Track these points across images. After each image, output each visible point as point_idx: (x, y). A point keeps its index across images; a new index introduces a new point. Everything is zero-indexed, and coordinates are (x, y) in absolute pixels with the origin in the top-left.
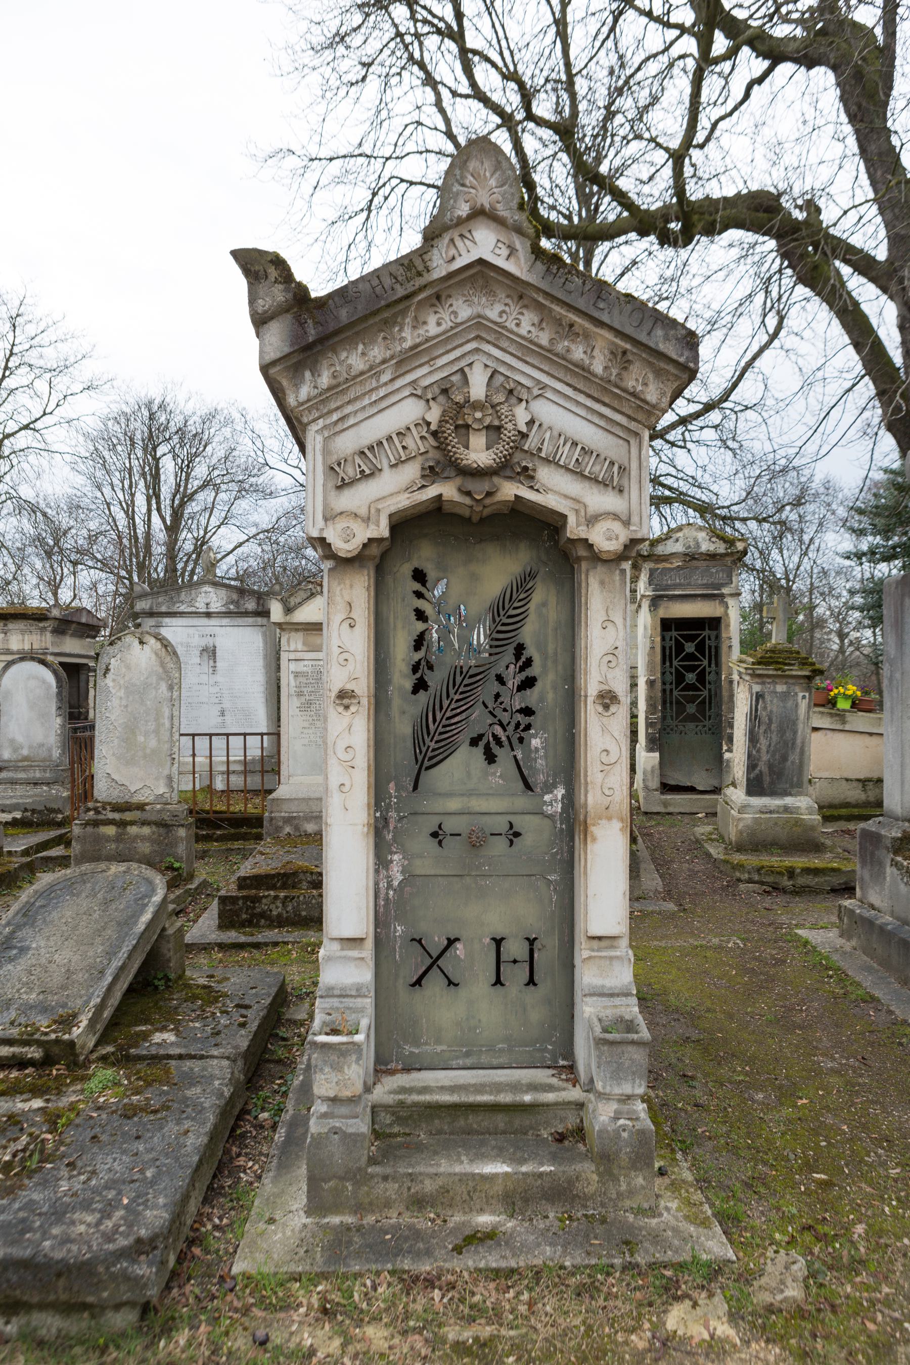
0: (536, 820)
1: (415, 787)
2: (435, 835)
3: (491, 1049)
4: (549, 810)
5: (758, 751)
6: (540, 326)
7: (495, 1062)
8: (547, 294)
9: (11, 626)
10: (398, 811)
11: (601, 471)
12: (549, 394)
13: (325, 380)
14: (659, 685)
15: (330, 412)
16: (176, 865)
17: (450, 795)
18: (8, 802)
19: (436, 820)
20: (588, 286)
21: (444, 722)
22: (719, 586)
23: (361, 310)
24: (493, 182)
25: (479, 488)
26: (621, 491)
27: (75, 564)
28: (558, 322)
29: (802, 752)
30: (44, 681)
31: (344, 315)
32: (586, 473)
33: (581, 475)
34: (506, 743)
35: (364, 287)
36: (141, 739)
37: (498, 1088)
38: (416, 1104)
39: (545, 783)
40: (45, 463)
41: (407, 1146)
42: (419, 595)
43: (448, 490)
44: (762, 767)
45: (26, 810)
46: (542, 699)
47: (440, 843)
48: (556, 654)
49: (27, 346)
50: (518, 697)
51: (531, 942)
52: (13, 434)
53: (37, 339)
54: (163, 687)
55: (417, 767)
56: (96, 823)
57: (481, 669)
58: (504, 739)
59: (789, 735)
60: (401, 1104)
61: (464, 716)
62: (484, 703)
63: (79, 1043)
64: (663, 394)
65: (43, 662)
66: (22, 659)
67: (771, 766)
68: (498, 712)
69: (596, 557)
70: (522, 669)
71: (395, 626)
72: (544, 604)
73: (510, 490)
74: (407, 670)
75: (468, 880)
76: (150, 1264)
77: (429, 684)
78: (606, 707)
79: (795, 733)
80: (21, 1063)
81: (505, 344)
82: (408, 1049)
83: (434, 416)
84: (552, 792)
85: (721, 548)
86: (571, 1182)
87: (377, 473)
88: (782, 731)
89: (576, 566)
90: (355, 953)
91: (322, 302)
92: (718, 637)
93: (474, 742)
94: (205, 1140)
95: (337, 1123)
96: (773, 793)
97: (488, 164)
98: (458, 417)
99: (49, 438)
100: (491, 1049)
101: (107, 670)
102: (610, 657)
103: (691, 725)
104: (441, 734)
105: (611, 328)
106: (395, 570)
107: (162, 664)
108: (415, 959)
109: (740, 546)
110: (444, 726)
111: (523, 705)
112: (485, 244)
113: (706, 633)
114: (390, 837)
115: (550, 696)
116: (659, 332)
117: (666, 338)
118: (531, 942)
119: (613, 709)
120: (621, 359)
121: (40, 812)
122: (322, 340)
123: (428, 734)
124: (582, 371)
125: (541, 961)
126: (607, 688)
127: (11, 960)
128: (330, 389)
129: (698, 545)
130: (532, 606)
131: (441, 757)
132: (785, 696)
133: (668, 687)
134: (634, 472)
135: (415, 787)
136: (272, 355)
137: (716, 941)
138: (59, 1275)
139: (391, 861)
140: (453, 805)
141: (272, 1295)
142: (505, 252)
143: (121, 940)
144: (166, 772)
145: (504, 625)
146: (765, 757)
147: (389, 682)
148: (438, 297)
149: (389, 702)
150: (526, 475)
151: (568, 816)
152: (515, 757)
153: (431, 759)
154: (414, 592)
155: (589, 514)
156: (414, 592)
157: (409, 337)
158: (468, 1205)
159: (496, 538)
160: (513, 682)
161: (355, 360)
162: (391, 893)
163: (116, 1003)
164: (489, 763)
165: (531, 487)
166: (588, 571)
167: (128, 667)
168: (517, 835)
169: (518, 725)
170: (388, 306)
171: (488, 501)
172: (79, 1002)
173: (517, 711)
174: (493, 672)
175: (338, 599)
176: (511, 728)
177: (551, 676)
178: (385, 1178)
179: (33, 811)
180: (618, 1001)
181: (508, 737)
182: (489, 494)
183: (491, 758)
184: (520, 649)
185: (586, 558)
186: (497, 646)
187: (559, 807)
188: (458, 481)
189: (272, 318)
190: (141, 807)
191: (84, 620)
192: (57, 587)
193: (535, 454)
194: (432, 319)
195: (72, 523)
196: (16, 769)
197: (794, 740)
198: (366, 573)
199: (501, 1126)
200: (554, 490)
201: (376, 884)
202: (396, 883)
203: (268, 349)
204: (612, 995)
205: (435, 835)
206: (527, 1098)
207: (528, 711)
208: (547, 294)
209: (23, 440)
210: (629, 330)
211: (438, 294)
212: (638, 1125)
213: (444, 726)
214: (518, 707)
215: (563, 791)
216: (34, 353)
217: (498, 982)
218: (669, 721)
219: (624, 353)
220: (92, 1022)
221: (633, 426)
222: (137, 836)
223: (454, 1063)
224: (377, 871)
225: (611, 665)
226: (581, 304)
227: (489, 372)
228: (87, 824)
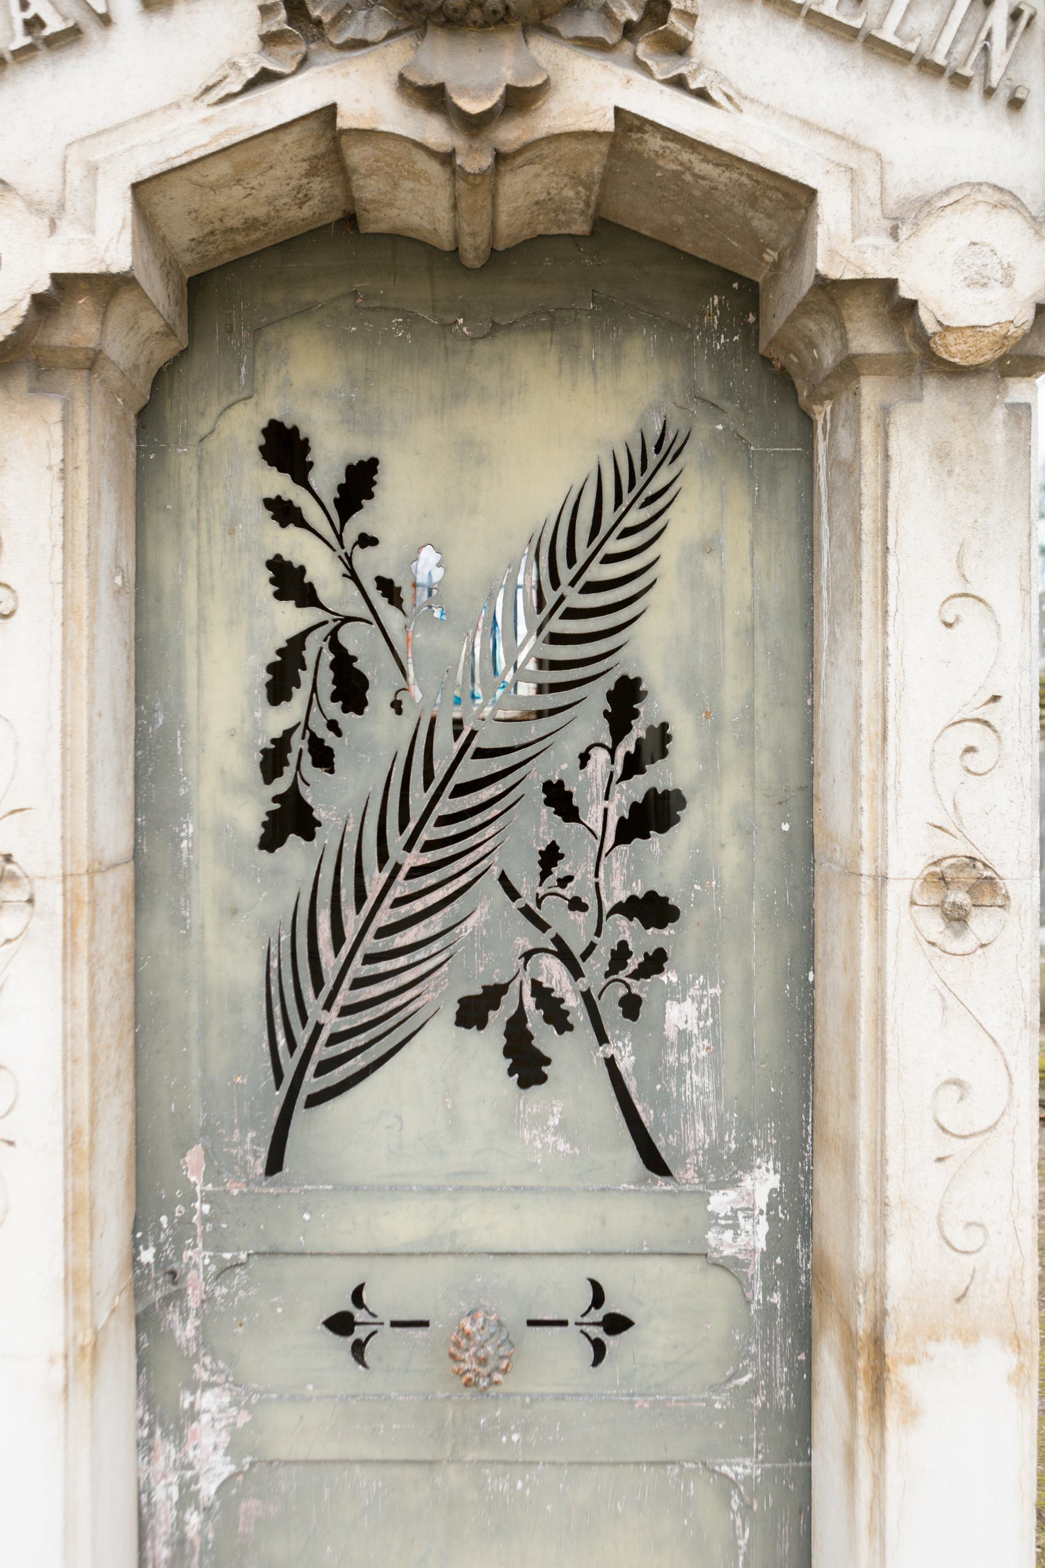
0: (682, 1275)
1: (275, 1164)
2: (340, 1324)
4: (725, 1243)
10: (215, 1243)
17: (393, 1190)
21: (371, 944)
26: (1016, 104)
32: (887, 35)
34: (579, 1015)
39: (713, 1154)
42: (284, 512)
47: (358, 1350)
48: (749, 713)
55: (281, 1094)
57: (496, 765)
58: (572, 1002)
61: (436, 923)
62: (503, 878)
68: (553, 911)
69: (921, 353)
70: (633, 766)
71: (202, 619)
72: (709, 546)
75: (453, 1477)
77: (319, 814)
78: (956, 918)
84: (735, 1183)
87: (92, 31)
89: (821, 413)
93: (472, 1013)
102: (973, 734)
104: (358, 983)
106: (203, 428)
110: (369, 959)
111: (639, 890)
115: (730, 858)
123: (318, 983)
126: (962, 848)
131: (359, 1063)
135: (275, 1164)
139: (193, 1415)
140: (402, 1224)
145: (572, 614)
147: (182, 808)
151: (792, 1261)
152: (610, 1063)
153: (324, 1067)
154: (268, 503)
155: (894, 194)
156: (268, 503)
159: (547, 320)
160: (603, 803)
162: (194, 1520)
164: (524, 1084)
165: (679, 83)
166: (886, 411)
169: (620, 955)
173: (613, 911)
174: (537, 775)
176: (596, 967)
177: (733, 791)
181: (587, 996)
182: (518, 100)
183: (527, 1066)
184: (626, 698)
185: (881, 365)
186: (555, 688)
187: (757, 1235)
198: (54, 409)
201: (143, 1489)
202: (208, 1488)
205: (340, 1324)
207: (653, 909)
213: (369, 959)
214: (622, 896)
215: (774, 1181)
224: (145, 1447)
225: (970, 760)
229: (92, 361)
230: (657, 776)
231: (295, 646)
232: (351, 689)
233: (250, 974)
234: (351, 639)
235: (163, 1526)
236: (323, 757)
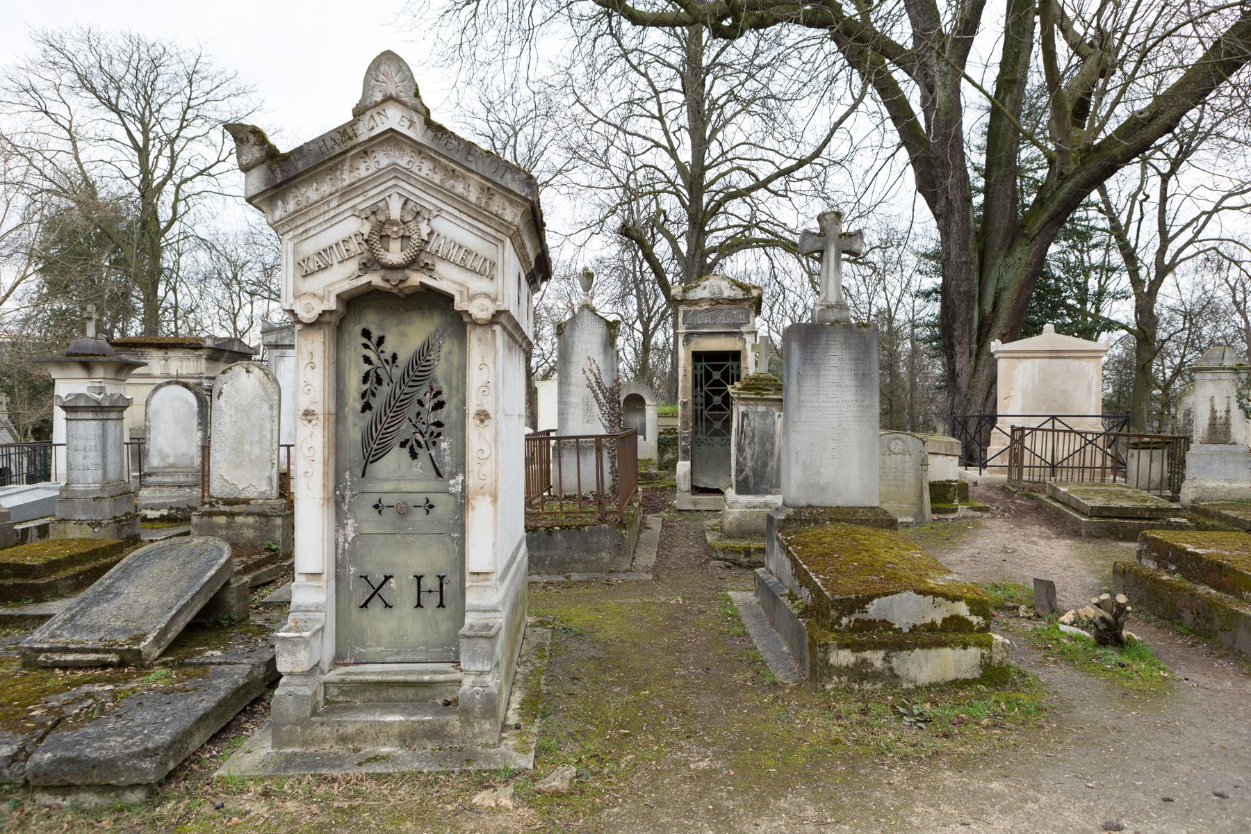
0: (444, 496)
1: (363, 475)
2: (376, 507)
3: (414, 650)
4: (453, 490)
5: (745, 459)
6: (434, 170)
7: (416, 659)
8: (436, 152)
9: (171, 354)
10: (351, 490)
11: (478, 265)
12: (444, 215)
13: (291, 207)
14: (690, 406)
15: (297, 227)
16: (274, 547)
17: (387, 480)
18: (157, 502)
19: (377, 497)
20: (462, 146)
22: (738, 326)
23: (312, 163)
24: (397, 79)
25: (396, 277)
27: (252, 294)
28: (445, 168)
29: (779, 460)
30: (187, 402)
31: (301, 166)
33: (464, 267)
35: (314, 147)
36: (247, 448)
37: (411, 672)
38: (353, 682)
40: (219, 207)
41: (345, 708)
42: (366, 346)
43: (375, 279)
44: (748, 471)
45: (171, 508)
46: (448, 416)
49: (203, 100)
50: (432, 414)
51: (441, 578)
52: (191, 179)
53: (212, 93)
54: (265, 406)
56: (210, 514)
59: (768, 446)
60: (343, 681)
63: (144, 652)
64: (516, 215)
65: (186, 386)
66: (169, 383)
67: (754, 471)
69: (475, 323)
70: (435, 396)
72: (450, 353)
73: (416, 278)
74: (358, 396)
76: (152, 762)
78: (482, 421)
79: (773, 444)
80: (104, 665)
81: (413, 182)
82: (358, 649)
83: (366, 228)
85: (739, 294)
86: (442, 727)
88: (763, 443)
90: (315, 583)
91: (286, 157)
92: (739, 367)
93: (403, 445)
94: (213, 705)
95: (291, 689)
96: (756, 492)
97: (393, 68)
98: (381, 232)
99: (223, 182)
100: (414, 650)
101: (221, 393)
103: (717, 439)
105: (478, 174)
107: (265, 389)
108: (364, 590)
109: (755, 293)
112: (393, 118)
113: (730, 363)
114: (346, 508)
116: (508, 176)
117: (513, 180)
118: (441, 578)
119: (486, 422)
120: (487, 192)
121: (183, 510)
122: (287, 181)
124: (461, 201)
125: (443, 591)
127: (107, 601)
128: (295, 212)
129: (721, 292)
130: (442, 354)
132: (764, 415)
133: (699, 408)
134: (500, 267)
135: (363, 475)
136: (253, 192)
137: (663, 599)
138: (94, 767)
140: (389, 486)
141: (237, 787)
142: (407, 124)
143: (190, 588)
144: (268, 474)
146: (750, 464)
147: (346, 405)
148: (366, 153)
149: (345, 418)
150: (428, 269)
157: (347, 178)
158: (376, 740)
160: (429, 405)
161: (311, 193)
163: (180, 630)
167: (237, 392)
168: (432, 507)
169: (432, 433)
170: (331, 159)
171: (402, 286)
172: (150, 627)
174: (416, 398)
175: (304, 350)
176: (427, 435)
178: (322, 724)
179: (178, 509)
180: (488, 615)
182: (401, 281)
183: (414, 455)
188: (382, 272)
189: (253, 167)
190: (246, 501)
191: (236, 349)
192: (235, 316)
193: (434, 255)
194: (363, 166)
195: (249, 257)
196: (164, 474)
197: (773, 450)
199: (411, 696)
200: (446, 278)
201: (337, 539)
203: (250, 187)
204: (485, 611)
205: (376, 507)
206: (426, 678)
207: (439, 424)
208: (436, 152)
209: (200, 184)
210: (488, 175)
211: (366, 150)
212: (487, 691)
216: (209, 106)
217: (419, 605)
218: (700, 435)
219: (489, 188)
220: (157, 640)
221: (499, 235)
222: (243, 524)
223: (389, 659)
224: (337, 531)
226: (457, 157)
227: (403, 200)
228: (203, 515)
229: (329, 323)
230: (440, 398)
231: (368, 373)
232: (379, 381)
233: (359, 437)
234: (379, 371)
235: (341, 545)
236: (374, 395)
